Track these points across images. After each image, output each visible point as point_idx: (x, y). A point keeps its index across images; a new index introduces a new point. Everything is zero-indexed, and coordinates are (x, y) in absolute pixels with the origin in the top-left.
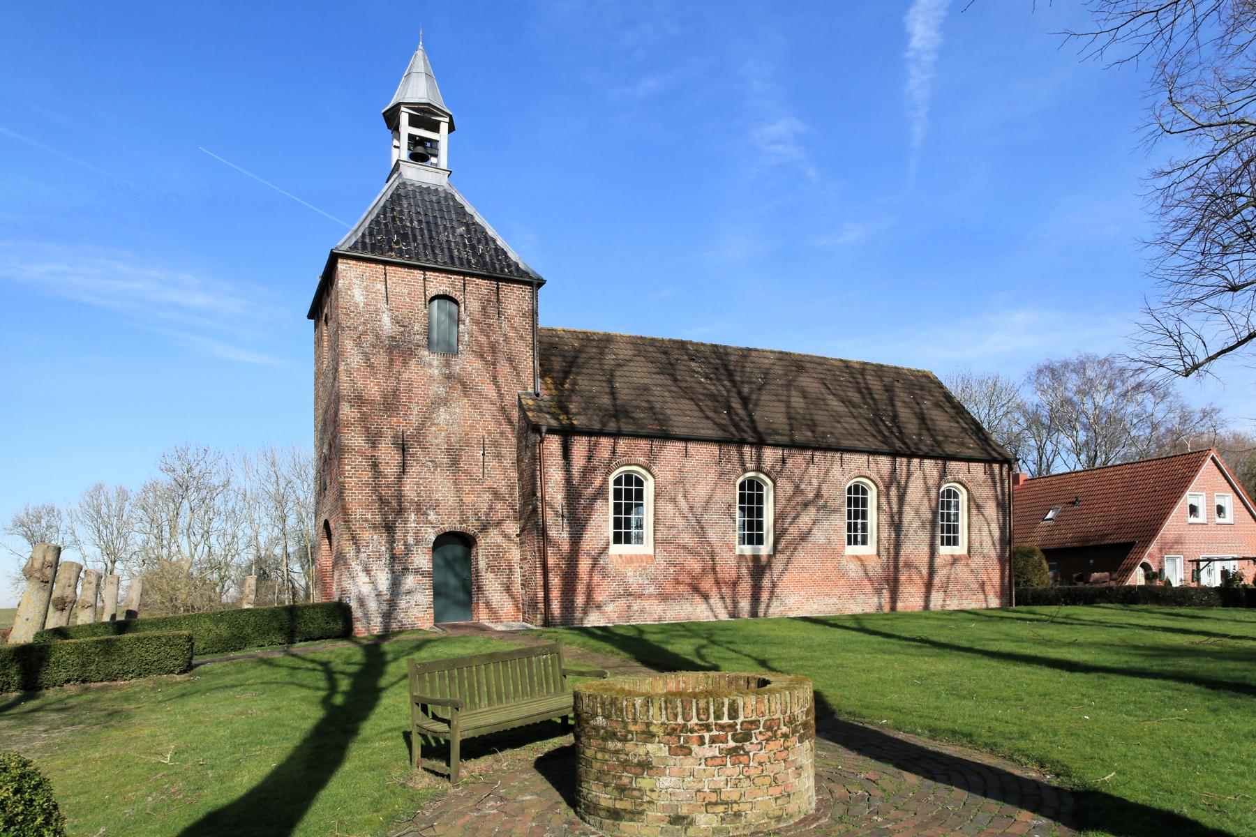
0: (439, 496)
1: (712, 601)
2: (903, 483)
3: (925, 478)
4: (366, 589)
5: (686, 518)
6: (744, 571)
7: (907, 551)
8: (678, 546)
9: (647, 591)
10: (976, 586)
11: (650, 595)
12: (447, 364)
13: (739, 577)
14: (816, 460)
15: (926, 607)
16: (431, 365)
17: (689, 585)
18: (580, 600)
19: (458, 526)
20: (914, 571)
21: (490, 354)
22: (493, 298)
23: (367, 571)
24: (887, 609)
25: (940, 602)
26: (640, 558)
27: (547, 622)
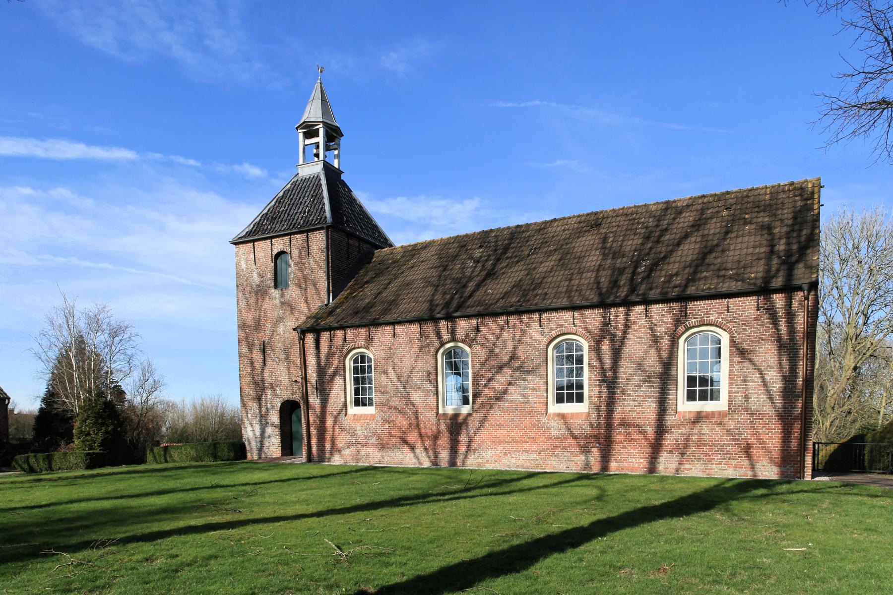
0: (281, 378)
1: (418, 451)
2: (619, 334)
3: (652, 328)
4: (251, 434)
5: (394, 385)
6: (443, 427)
7: (625, 408)
8: (390, 408)
9: (371, 441)
10: (737, 449)
11: (373, 444)
12: (282, 295)
13: (439, 432)
14: (511, 324)
15: (652, 469)
16: (275, 298)
17: (400, 438)
18: (328, 446)
19: (291, 396)
20: (634, 432)
21: (304, 283)
22: (305, 245)
23: (251, 424)
24: (596, 469)
25: (673, 466)
26: (365, 417)
27: (310, 459)
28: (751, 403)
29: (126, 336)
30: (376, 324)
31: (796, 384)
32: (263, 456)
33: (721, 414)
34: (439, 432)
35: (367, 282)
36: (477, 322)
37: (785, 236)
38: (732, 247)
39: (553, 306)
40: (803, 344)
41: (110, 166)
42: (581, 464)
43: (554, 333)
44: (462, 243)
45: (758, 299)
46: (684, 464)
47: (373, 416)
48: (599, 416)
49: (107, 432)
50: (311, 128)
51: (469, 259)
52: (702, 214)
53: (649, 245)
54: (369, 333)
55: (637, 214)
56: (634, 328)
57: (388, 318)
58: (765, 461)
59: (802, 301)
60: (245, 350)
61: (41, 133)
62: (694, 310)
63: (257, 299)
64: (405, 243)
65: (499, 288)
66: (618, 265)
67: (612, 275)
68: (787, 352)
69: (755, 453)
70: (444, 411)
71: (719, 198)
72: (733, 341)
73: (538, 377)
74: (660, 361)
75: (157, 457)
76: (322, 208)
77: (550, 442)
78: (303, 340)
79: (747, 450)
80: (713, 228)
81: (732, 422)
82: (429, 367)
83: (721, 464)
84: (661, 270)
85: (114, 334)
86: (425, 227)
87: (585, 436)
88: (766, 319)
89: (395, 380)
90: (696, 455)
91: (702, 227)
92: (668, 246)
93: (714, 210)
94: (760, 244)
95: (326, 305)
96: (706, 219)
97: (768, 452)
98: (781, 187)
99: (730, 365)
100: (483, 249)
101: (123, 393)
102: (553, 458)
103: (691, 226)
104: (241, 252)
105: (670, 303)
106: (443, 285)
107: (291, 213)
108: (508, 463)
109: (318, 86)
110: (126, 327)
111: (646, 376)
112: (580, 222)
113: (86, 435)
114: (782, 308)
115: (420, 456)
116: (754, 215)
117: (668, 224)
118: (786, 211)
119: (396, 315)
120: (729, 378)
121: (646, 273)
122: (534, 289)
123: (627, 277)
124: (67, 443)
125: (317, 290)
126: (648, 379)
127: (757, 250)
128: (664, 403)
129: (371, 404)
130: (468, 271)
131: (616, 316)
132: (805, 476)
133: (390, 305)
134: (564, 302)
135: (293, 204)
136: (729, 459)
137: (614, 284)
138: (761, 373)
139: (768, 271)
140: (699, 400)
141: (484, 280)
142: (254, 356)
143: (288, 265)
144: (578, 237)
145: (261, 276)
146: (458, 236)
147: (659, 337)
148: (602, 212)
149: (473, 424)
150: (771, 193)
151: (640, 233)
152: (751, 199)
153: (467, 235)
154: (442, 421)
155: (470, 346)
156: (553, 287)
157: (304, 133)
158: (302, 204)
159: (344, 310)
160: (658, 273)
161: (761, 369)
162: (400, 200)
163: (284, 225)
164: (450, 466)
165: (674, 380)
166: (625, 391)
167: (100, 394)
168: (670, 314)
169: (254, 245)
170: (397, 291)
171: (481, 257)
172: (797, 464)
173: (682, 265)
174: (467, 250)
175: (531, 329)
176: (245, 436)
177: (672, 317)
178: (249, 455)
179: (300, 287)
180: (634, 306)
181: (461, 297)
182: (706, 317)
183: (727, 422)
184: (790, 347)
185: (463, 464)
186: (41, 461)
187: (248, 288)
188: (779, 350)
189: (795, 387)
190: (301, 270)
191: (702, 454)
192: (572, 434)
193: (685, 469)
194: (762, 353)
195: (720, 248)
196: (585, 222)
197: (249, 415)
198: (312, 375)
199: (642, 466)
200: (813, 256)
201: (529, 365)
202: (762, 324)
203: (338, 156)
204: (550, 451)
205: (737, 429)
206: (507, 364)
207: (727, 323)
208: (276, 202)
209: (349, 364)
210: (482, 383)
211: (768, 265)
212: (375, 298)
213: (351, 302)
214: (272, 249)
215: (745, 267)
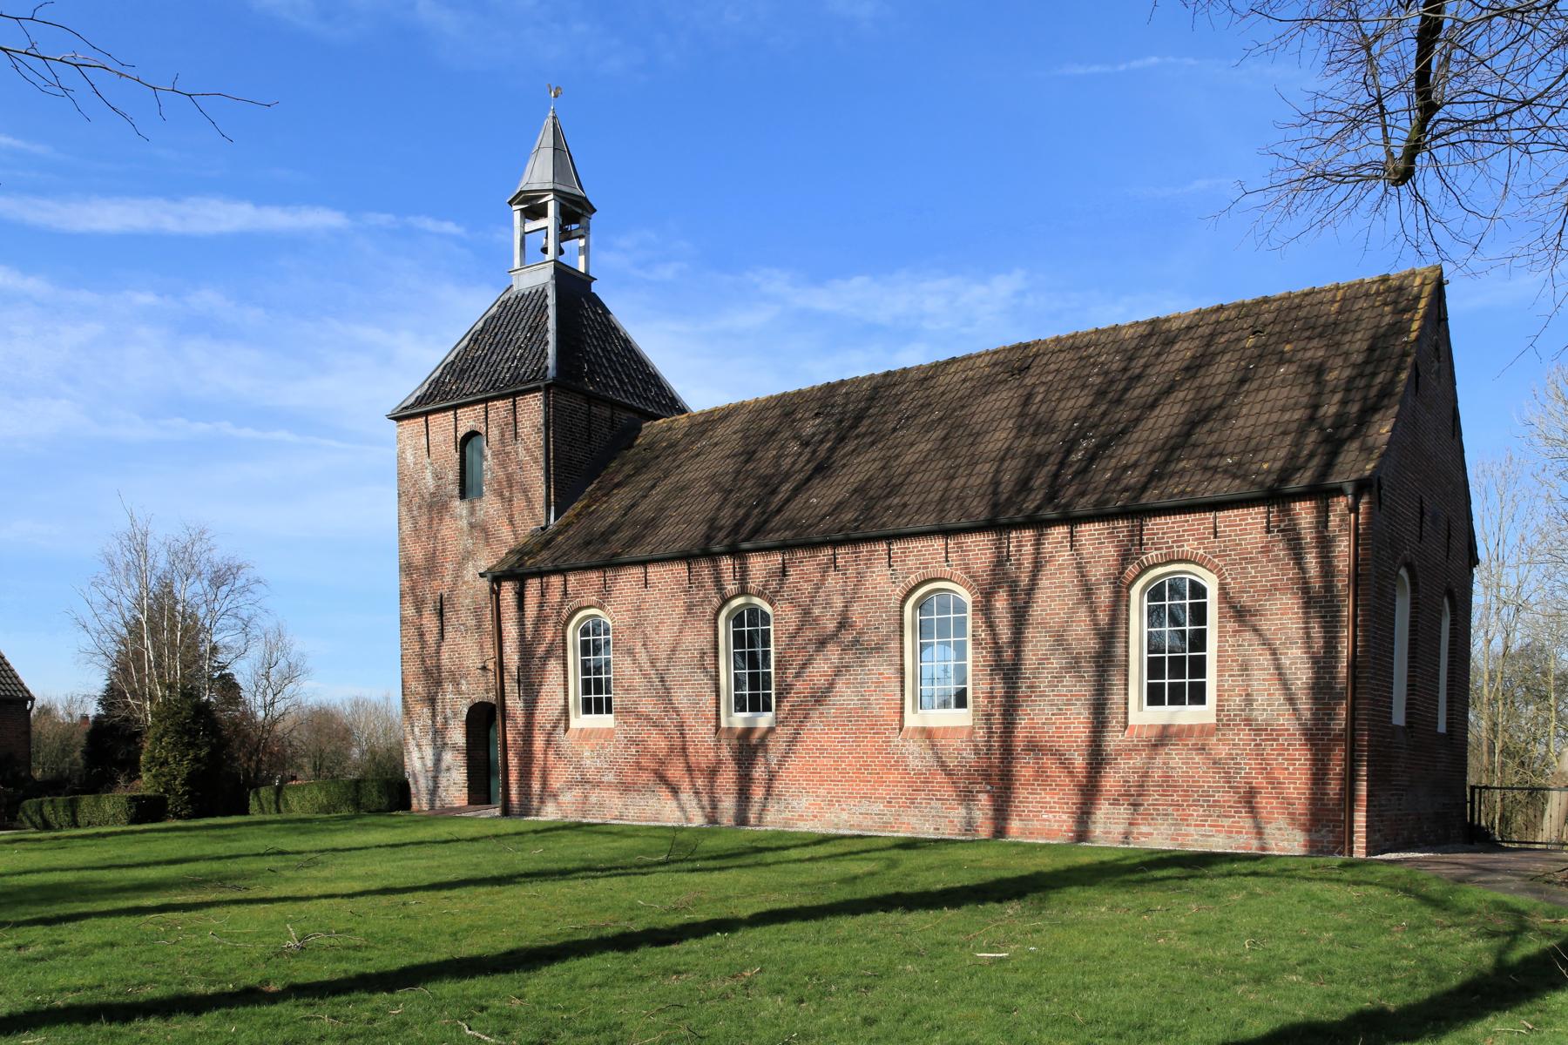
2: (1025, 580)
3: (1081, 569)
4: (418, 764)
6: (726, 753)
7: (1035, 718)
8: (639, 716)
10: (1231, 798)
11: (610, 784)
12: (472, 512)
15: (1082, 834)
16: (461, 517)
17: (656, 772)
18: (536, 786)
21: (509, 487)
22: (511, 419)
23: (418, 746)
24: (984, 831)
25: (1119, 829)
27: (506, 812)
28: (1258, 710)
29: (238, 584)
30: (613, 564)
31: (1336, 672)
32: (438, 804)
33: (1205, 731)
34: (719, 762)
35: (618, 485)
36: (783, 560)
37: (1343, 387)
38: (1244, 411)
39: (911, 528)
40: (1348, 595)
41: (295, 244)
42: (961, 822)
43: (913, 579)
44: (787, 408)
45: (1269, 512)
46: (1138, 824)
47: (610, 732)
48: (990, 732)
49: (196, 759)
50: (534, 202)
51: (794, 438)
52: (1208, 345)
53: (1103, 407)
54: (605, 580)
55: (1096, 345)
56: (1049, 569)
57: (638, 553)
58: (1281, 821)
59: (1344, 515)
60: (410, 611)
61: (173, 187)
62: (1154, 534)
63: (431, 520)
64: (708, 407)
65: (831, 495)
66: (1039, 449)
67: (1024, 468)
68: (1320, 612)
69: (1264, 805)
70: (729, 722)
71: (1245, 310)
72: (1223, 589)
73: (886, 661)
74: (1095, 629)
75: (265, 805)
76: (543, 350)
77: (906, 782)
78: (498, 594)
79: (1249, 799)
80: (1222, 372)
81: (1223, 745)
82: (704, 642)
83: (1204, 826)
84: (1111, 457)
85: (218, 580)
86: (906, 334)
87: (967, 770)
88: (1283, 550)
89: (647, 666)
90: (1161, 808)
91: (1203, 371)
92: (1133, 409)
93: (1234, 336)
94: (1295, 404)
95: (542, 528)
96: (1215, 354)
97: (1288, 804)
98: (1366, 287)
99: (1219, 637)
100: (821, 419)
101: (236, 686)
102: (912, 811)
103: (1183, 370)
104: (406, 435)
105: (1113, 520)
106: (739, 489)
107: (492, 361)
108: (836, 820)
109: (549, 122)
110: (239, 568)
111: (1072, 658)
112: (995, 364)
113: (162, 765)
114: (1310, 528)
115: (688, 806)
116: (1301, 344)
117: (1146, 366)
118: (1359, 336)
119: (649, 548)
120: (1218, 661)
121: (1084, 464)
122: (887, 496)
123: (1049, 471)
124: (131, 780)
125: (529, 500)
126: (1074, 665)
127: (1287, 416)
128: (1104, 709)
129: (609, 711)
130: (786, 463)
131: (1019, 546)
132: (1355, 849)
133: (646, 528)
134: (928, 521)
135: (498, 342)
136: (1218, 816)
137: (1024, 485)
138: (1274, 653)
139: (1293, 457)
140: (1169, 704)
141: (809, 479)
142: (425, 621)
143: (482, 456)
144: (985, 394)
145: (438, 477)
146: (784, 395)
147: (1094, 584)
148: (1037, 343)
149: (776, 746)
150: (1344, 299)
151: (1093, 385)
152: (1302, 314)
153: (799, 393)
154: (724, 742)
155: (772, 604)
156: (921, 493)
157: (522, 210)
158: (513, 344)
159: (569, 538)
160: (1103, 464)
161: (1275, 644)
162: (858, 281)
163: (478, 383)
164: (738, 825)
165: (1120, 666)
166: (1036, 687)
167: (189, 694)
168: (1113, 542)
169: (426, 421)
170: (662, 501)
171: (814, 435)
172: (1340, 827)
173: (1149, 447)
174: (793, 421)
175: (874, 572)
176: (408, 769)
177: (1117, 546)
178: (414, 801)
179: (501, 495)
180: (1050, 527)
181: (763, 513)
182: (1178, 547)
183: (1215, 745)
184: (1326, 602)
185: (760, 819)
186: (61, 809)
187: (417, 500)
188: (1306, 608)
189: (1335, 678)
190: (503, 465)
191: (1171, 805)
192: (943, 766)
193: (1140, 834)
194: (1277, 614)
195: (1223, 413)
196: (1003, 363)
197: (416, 729)
198: (512, 659)
199: (1065, 828)
200: (1380, 428)
201: (871, 638)
202: (1276, 559)
203: (585, 250)
204: (907, 799)
205: (1233, 759)
206: (834, 636)
207: (1214, 557)
208: (471, 340)
209: (573, 636)
210: (791, 671)
211: (1297, 444)
212: (625, 514)
213: (584, 521)
214: (456, 428)
215: (1256, 451)
